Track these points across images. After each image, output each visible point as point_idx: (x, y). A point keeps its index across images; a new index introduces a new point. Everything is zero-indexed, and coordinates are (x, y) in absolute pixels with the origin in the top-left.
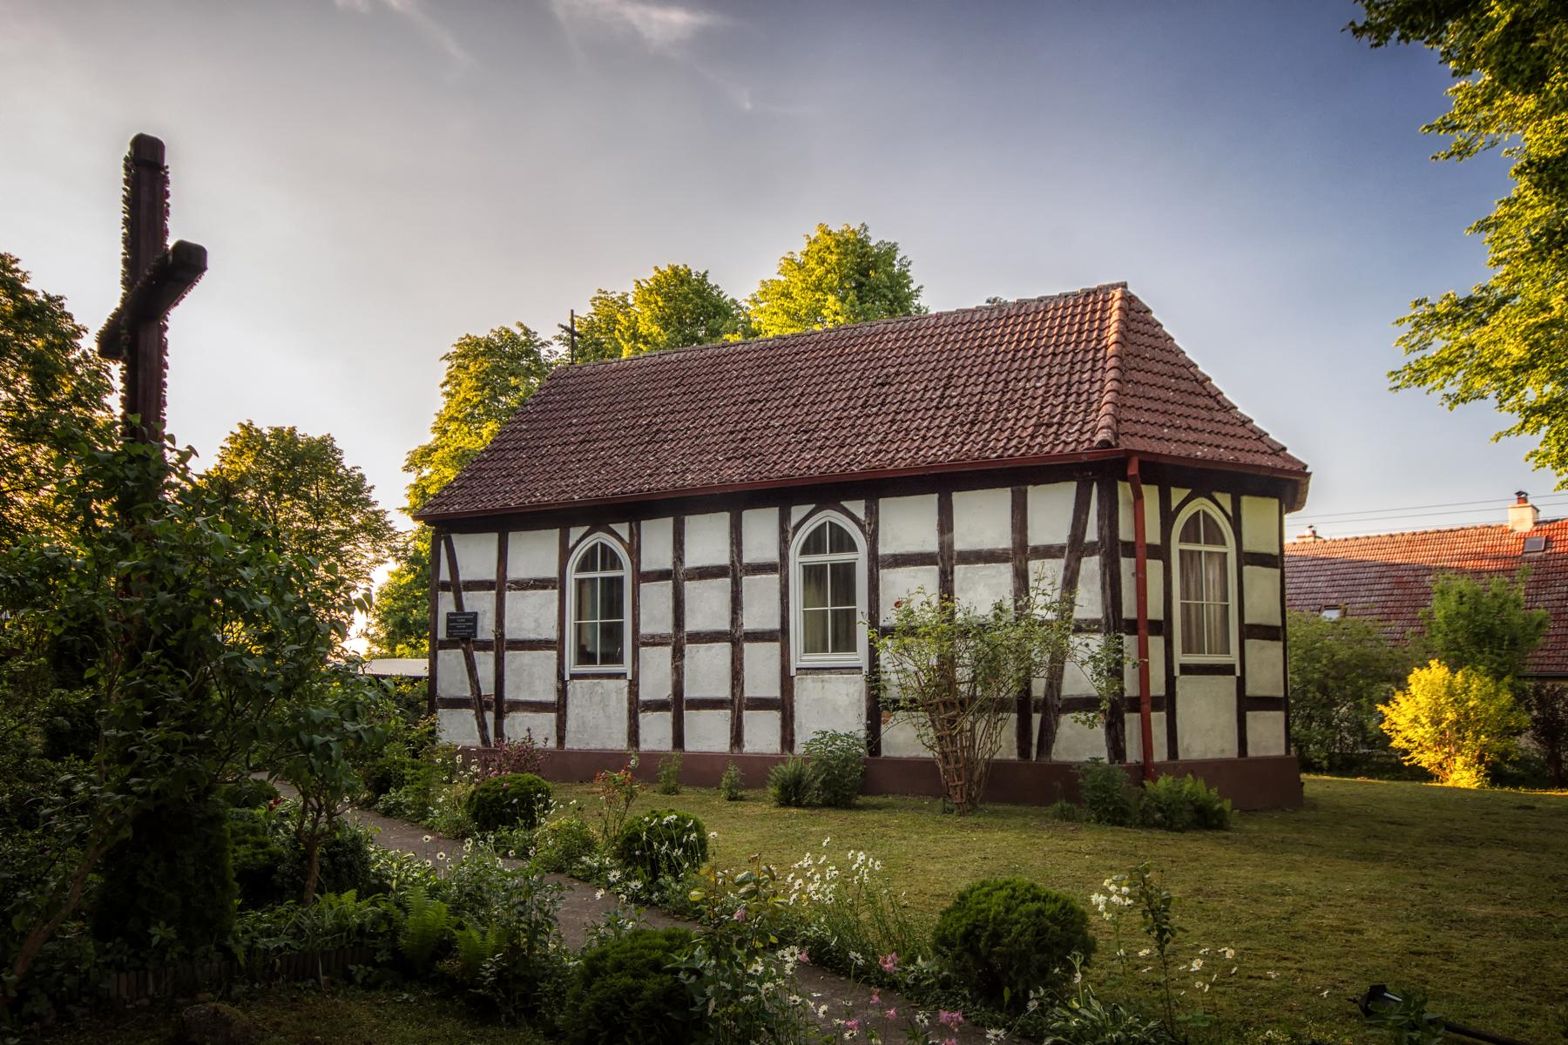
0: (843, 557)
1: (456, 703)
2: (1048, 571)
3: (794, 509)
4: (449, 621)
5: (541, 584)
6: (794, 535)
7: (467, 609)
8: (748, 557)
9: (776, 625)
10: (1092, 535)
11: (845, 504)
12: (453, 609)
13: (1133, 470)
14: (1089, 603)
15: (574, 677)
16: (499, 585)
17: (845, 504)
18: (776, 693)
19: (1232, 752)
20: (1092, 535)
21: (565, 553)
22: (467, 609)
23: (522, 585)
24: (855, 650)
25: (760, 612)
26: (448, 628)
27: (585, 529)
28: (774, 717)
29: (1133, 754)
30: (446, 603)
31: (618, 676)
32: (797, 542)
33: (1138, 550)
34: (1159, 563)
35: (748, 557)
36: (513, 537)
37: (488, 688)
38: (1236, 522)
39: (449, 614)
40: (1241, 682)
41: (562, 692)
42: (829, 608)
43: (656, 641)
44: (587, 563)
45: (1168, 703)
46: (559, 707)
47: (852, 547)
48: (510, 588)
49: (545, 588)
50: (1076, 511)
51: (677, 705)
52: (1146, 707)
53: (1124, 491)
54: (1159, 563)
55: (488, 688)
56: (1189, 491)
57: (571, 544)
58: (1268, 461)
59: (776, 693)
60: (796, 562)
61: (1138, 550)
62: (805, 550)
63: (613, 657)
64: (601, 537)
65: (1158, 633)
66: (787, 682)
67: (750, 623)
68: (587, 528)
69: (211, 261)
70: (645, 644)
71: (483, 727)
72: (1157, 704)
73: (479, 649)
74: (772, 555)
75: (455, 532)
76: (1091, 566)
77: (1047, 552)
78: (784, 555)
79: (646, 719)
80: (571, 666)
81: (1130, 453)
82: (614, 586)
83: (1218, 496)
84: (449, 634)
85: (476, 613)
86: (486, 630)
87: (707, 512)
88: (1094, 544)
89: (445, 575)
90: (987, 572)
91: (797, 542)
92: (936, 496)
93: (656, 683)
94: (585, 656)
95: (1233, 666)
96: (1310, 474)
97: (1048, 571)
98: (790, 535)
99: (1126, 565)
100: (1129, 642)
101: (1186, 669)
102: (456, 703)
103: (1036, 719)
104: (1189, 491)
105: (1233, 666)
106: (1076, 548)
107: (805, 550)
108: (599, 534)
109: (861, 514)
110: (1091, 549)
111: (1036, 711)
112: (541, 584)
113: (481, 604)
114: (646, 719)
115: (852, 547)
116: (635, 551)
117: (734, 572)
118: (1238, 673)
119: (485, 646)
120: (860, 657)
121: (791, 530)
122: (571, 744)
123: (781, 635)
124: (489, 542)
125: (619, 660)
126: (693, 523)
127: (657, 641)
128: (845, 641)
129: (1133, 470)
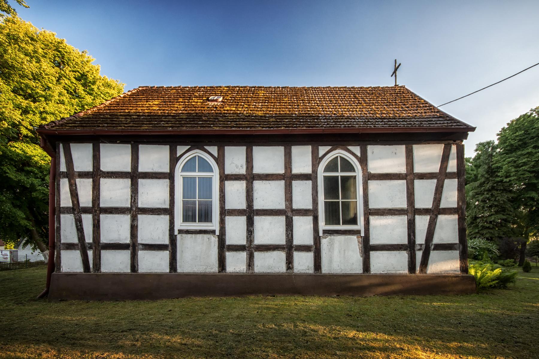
3: (179, 147)
9: (167, 206)
11: (206, 147)
17: (350, 148)
24: (211, 221)
40: (366, 240)
42: (340, 200)
44: (332, 166)
47: (211, 170)
59: (167, 242)
60: (321, 174)
62: (183, 170)
66: (317, 239)
68: (189, 147)
74: (308, 170)
78: (315, 171)
80: (322, 225)
87: (382, 145)
94: (188, 217)
104: (217, 157)
107: (327, 169)
108: (337, 151)
109: (215, 153)
115: (211, 170)
122: (325, 269)
123: (313, 213)
124: (279, 151)
125: (354, 221)
126: (296, 150)
128: (206, 216)
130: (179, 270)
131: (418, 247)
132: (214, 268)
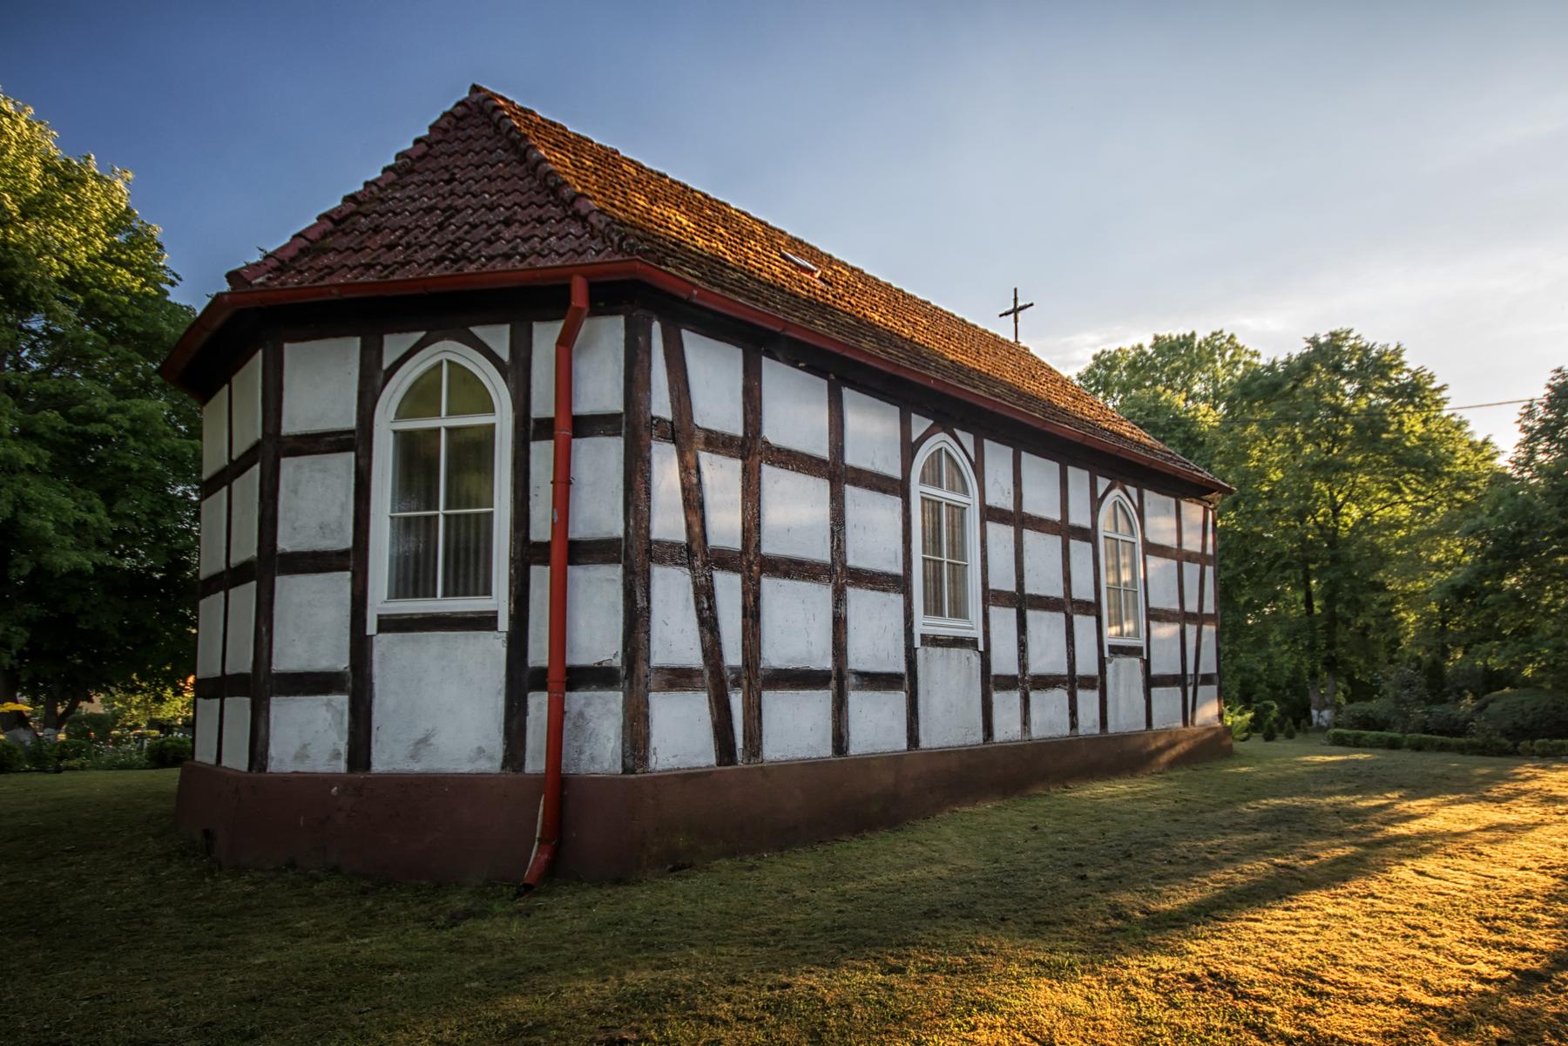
0: (957, 498)
15: (389, 624)
17: (478, 331)
18: (342, 663)
19: (977, 737)
31: (485, 622)
40: (1147, 665)
52: (555, 676)
64: (449, 351)
65: (1086, 613)
75: (1071, 465)
83: (1129, 488)
90: (896, 515)
92: (507, 327)
95: (1141, 649)
96: (232, 276)
100: (1191, 630)
101: (933, 641)
103: (736, 700)
105: (1141, 649)
118: (981, 648)
120: (499, 601)
130: (924, 743)
131: (1189, 681)
132: (1066, 731)
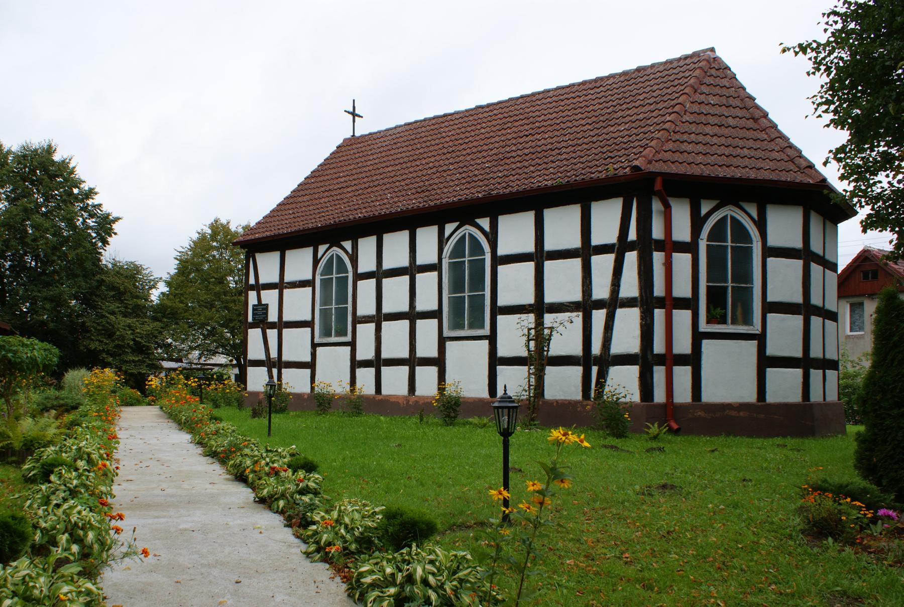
1: (257, 363)
2: (603, 264)
4: (254, 309)
5: (303, 284)
6: (446, 244)
7: (263, 302)
8: (420, 261)
10: (632, 235)
12: (256, 303)
13: (658, 186)
14: (630, 287)
16: (281, 286)
20: (632, 235)
21: (316, 262)
22: (263, 302)
23: (294, 285)
25: (427, 301)
26: (253, 314)
27: (327, 246)
28: (433, 371)
29: (659, 396)
30: (252, 297)
32: (448, 248)
33: (670, 246)
34: (688, 257)
35: (420, 261)
36: (289, 254)
37: (274, 354)
38: (761, 225)
39: (254, 306)
41: (314, 355)
43: (366, 320)
45: (694, 360)
46: (311, 365)
48: (286, 287)
49: (300, 282)
50: (622, 218)
51: (378, 363)
53: (657, 206)
54: (688, 257)
55: (274, 354)
56: (718, 201)
57: (319, 256)
58: (799, 178)
61: (670, 246)
63: (342, 332)
67: (420, 307)
69: (725, 55)
70: (360, 323)
71: (271, 376)
72: (682, 360)
73: (269, 328)
74: (434, 259)
76: (631, 258)
77: (604, 249)
79: (360, 372)
81: (654, 175)
82: (343, 282)
84: (254, 318)
85: (267, 305)
86: (273, 317)
88: (633, 242)
89: (252, 281)
91: (448, 248)
93: (365, 351)
97: (603, 264)
98: (444, 244)
99: (658, 258)
102: (257, 363)
103: (595, 369)
106: (620, 248)
110: (631, 247)
111: (595, 365)
112: (303, 284)
113: (270, 297)
114: (360, 372)
116: (354, 259)
117: (412, 270)
119: (272, 326)
121: (445, 241)
127: (367, 319)
129: (658, 186)
